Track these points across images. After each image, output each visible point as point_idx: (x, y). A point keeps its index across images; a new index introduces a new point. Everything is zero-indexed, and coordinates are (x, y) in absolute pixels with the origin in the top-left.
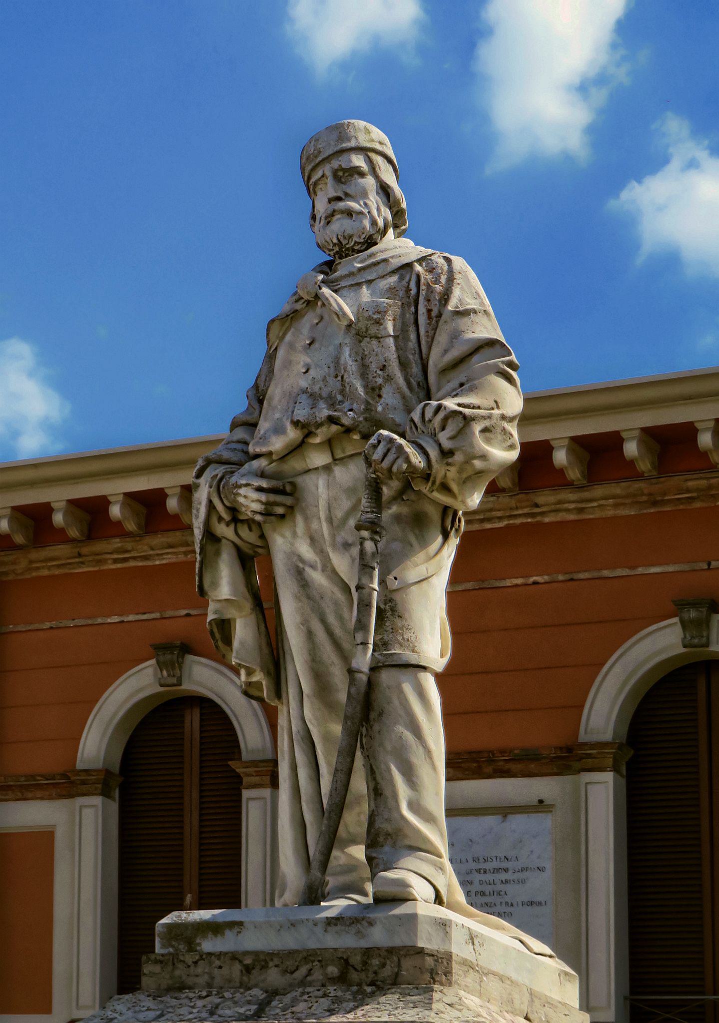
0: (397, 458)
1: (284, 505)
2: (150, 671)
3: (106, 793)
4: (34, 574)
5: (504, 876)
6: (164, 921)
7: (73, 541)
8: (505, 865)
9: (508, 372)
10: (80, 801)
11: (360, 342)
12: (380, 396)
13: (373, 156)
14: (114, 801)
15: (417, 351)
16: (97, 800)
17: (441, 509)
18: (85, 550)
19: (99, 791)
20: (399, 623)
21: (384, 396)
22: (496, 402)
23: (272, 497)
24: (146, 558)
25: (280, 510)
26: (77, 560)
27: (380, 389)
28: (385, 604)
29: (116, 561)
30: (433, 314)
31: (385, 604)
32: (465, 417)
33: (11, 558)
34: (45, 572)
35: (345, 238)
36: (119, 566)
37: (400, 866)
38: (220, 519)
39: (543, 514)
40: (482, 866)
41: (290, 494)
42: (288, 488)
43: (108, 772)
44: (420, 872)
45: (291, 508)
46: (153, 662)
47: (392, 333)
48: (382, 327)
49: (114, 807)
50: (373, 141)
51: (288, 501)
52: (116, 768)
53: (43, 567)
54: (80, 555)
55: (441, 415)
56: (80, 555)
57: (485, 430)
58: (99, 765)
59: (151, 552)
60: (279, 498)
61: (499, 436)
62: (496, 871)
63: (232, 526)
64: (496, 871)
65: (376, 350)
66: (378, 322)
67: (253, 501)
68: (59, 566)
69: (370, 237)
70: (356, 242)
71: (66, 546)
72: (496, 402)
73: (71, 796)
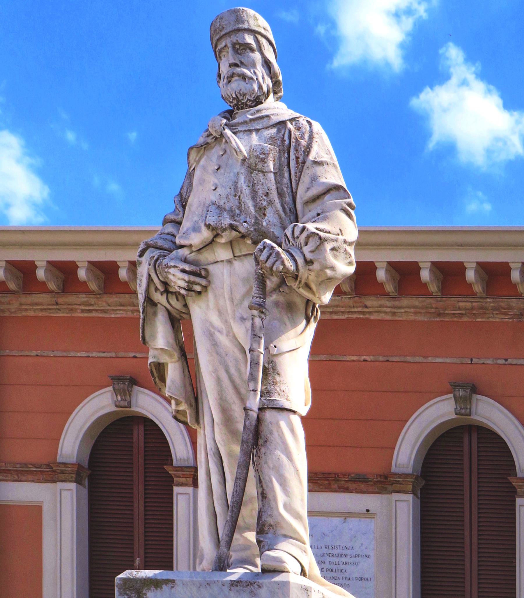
0: (276, 261)
1: (200, 285)
2: (109, 395)
3: (78, 481)
4: (24, 314)
5: (344, 560)
6: (121, 576)
7: (52, 292)
8: (345, 552)
9: (348, 210)
10: (60, 485)
11: (251, 173)
12: (265, 215)
13: (259, 37)
14: (85, 487)
15: (289, 186)
16: (73, 486)
17: (305, 301)
18: (61, 300)
19: (74, 480)
20: (278, 378)
21: (267, 215)
22: (340, 230)
23: (192, 278)
24: (104, 311)
25: (198, 288)
26: (55, 307)
27: (265, 209)
28: (269, 364)
29: (83, 311)
30: (300, 160)
31: (269, 364)
32: (320, 238)
33: (7, 300)
34: (32, 314)
35: (241, 95)
36: (86, 315)
37: (278, 548)
38: (157, 289)
39: (370, 313)
40: (330, 551)
41: (205, 278)
42: (203, 273)
43: (80, 466)
44: (289, 552)
45: (205, 288)
46: (111, 388)
47: (272, 170)
48: (266, 165)
49: (85, 492)
50: (259, 26)
51: (204, 282)
52: (86, 464)
53: (30, 309)
54: (57, 304)
55: (305, 234)
56: (57, 304)
57: (333, 249)
58: (73, 460)
59: (108, 308)
60: (197, 279)
61: (342, 254)
62: (340, 555)
63: (165, 295)
64: (340, 555)
65: (262, 181)
66: (263, 161)
67: (179, 279)
68: (42, 310)
69: (258, 97)
70: (248, 99)
71: (47, 296)
72: (340, 230)
73: (54, 481)
